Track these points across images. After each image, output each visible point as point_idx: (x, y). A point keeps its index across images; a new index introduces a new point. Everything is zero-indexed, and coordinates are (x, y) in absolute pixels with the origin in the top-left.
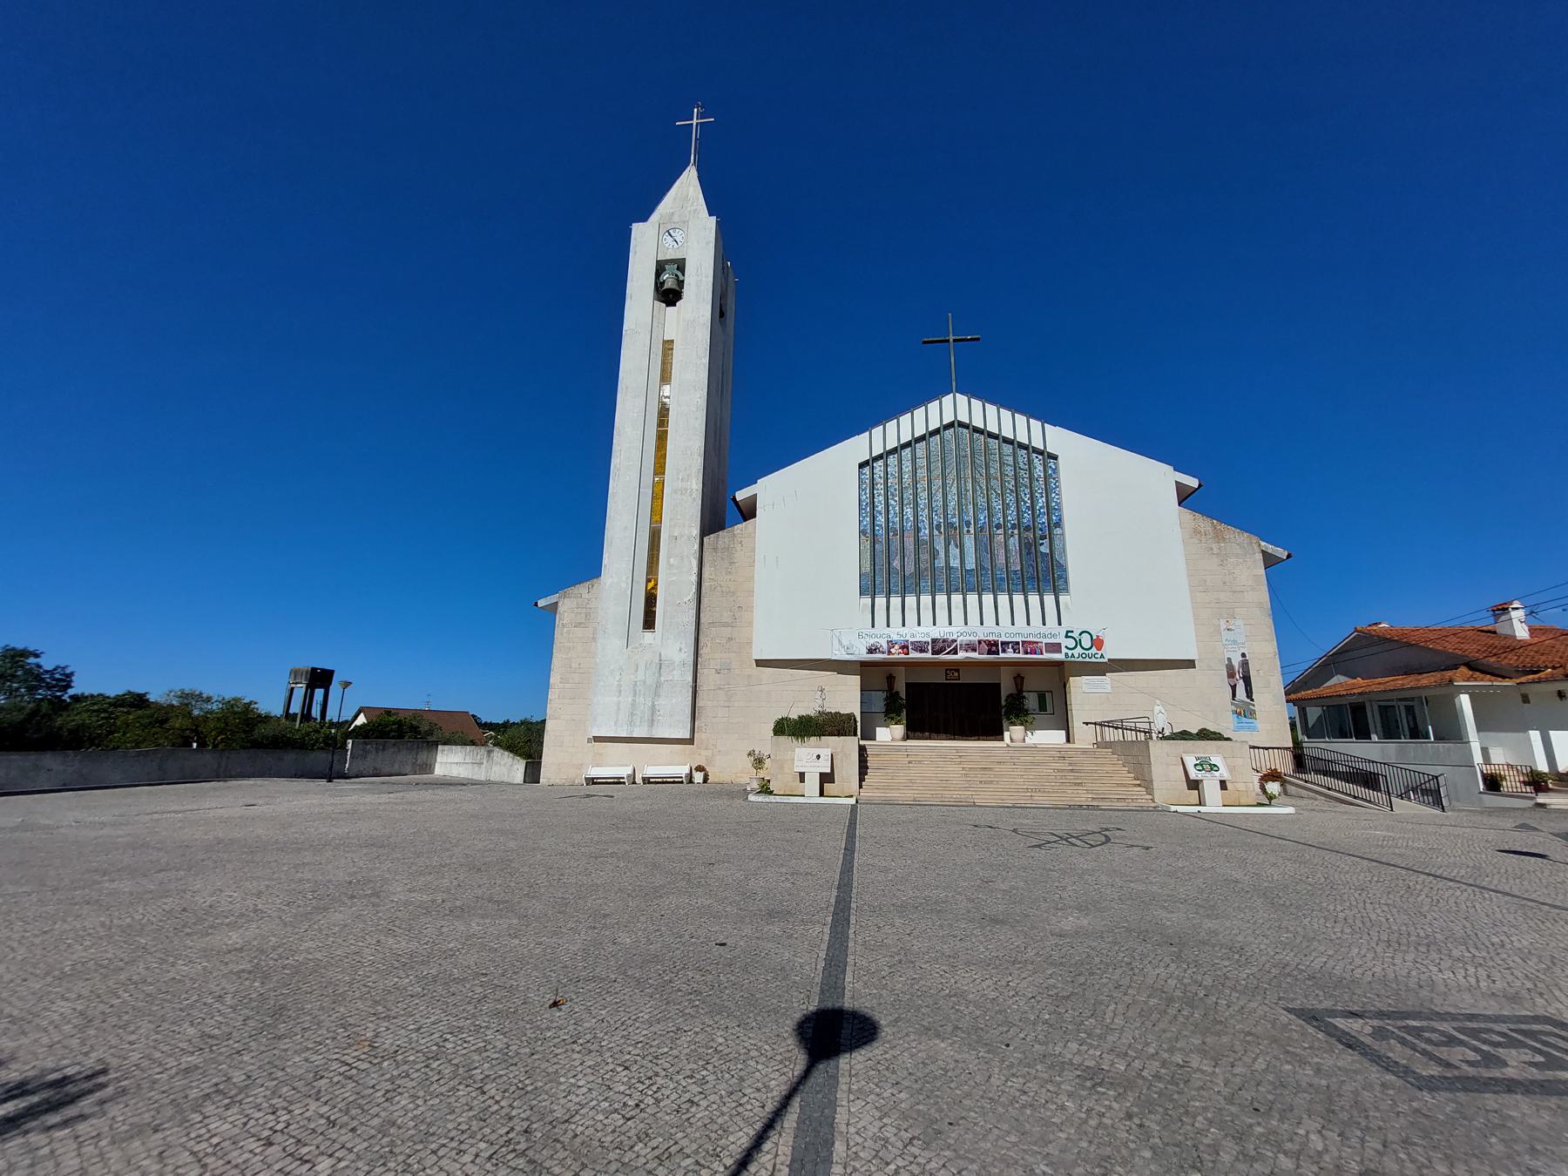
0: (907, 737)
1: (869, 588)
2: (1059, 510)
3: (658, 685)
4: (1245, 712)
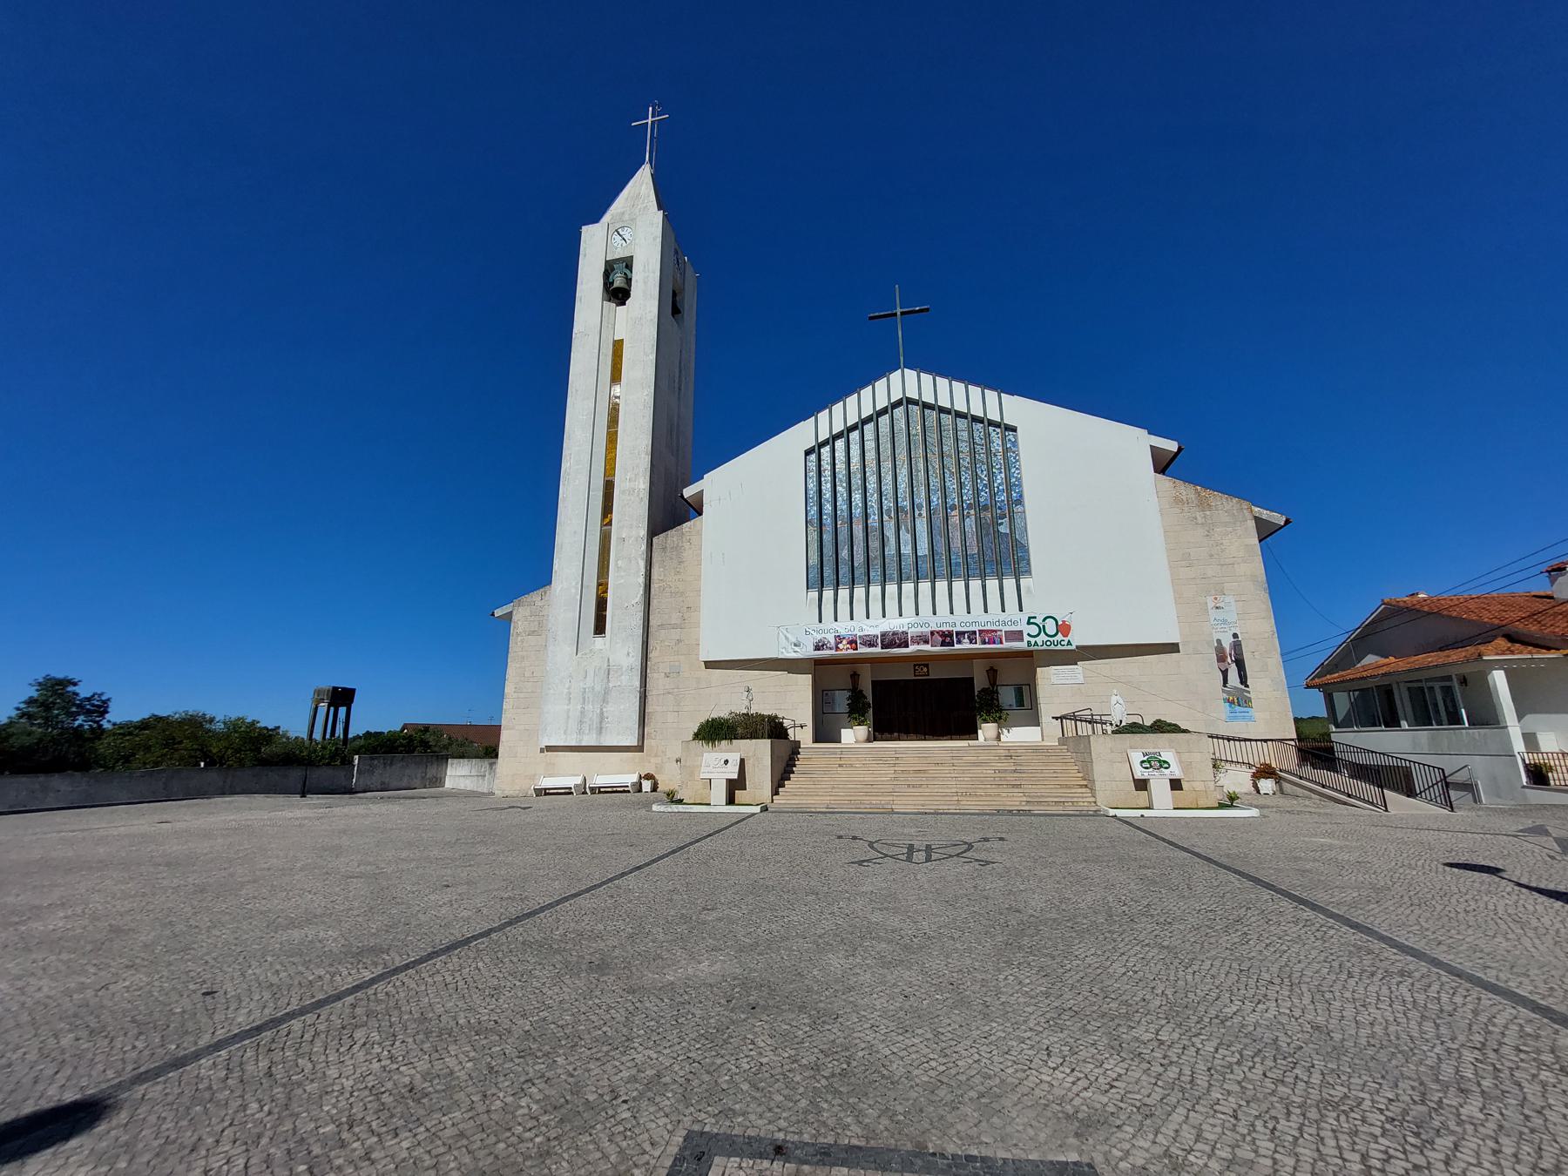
0: (868, 740)
2: (1020, 485)
3: (607, 692)
4: (1239, 700)
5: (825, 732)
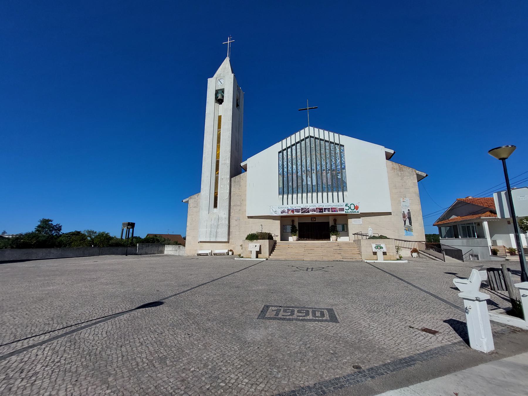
0: (297, 240)
1: (282, 192)
3: (218, 225)
4: (409, 230)
5: (284, 238)
